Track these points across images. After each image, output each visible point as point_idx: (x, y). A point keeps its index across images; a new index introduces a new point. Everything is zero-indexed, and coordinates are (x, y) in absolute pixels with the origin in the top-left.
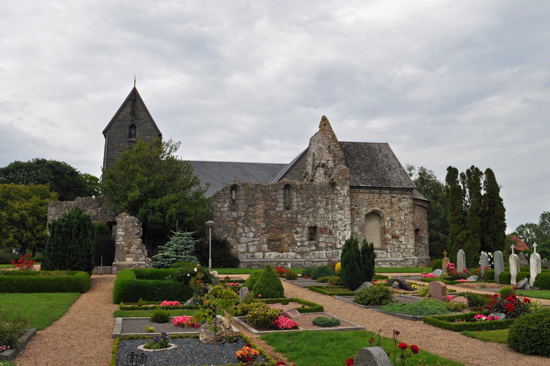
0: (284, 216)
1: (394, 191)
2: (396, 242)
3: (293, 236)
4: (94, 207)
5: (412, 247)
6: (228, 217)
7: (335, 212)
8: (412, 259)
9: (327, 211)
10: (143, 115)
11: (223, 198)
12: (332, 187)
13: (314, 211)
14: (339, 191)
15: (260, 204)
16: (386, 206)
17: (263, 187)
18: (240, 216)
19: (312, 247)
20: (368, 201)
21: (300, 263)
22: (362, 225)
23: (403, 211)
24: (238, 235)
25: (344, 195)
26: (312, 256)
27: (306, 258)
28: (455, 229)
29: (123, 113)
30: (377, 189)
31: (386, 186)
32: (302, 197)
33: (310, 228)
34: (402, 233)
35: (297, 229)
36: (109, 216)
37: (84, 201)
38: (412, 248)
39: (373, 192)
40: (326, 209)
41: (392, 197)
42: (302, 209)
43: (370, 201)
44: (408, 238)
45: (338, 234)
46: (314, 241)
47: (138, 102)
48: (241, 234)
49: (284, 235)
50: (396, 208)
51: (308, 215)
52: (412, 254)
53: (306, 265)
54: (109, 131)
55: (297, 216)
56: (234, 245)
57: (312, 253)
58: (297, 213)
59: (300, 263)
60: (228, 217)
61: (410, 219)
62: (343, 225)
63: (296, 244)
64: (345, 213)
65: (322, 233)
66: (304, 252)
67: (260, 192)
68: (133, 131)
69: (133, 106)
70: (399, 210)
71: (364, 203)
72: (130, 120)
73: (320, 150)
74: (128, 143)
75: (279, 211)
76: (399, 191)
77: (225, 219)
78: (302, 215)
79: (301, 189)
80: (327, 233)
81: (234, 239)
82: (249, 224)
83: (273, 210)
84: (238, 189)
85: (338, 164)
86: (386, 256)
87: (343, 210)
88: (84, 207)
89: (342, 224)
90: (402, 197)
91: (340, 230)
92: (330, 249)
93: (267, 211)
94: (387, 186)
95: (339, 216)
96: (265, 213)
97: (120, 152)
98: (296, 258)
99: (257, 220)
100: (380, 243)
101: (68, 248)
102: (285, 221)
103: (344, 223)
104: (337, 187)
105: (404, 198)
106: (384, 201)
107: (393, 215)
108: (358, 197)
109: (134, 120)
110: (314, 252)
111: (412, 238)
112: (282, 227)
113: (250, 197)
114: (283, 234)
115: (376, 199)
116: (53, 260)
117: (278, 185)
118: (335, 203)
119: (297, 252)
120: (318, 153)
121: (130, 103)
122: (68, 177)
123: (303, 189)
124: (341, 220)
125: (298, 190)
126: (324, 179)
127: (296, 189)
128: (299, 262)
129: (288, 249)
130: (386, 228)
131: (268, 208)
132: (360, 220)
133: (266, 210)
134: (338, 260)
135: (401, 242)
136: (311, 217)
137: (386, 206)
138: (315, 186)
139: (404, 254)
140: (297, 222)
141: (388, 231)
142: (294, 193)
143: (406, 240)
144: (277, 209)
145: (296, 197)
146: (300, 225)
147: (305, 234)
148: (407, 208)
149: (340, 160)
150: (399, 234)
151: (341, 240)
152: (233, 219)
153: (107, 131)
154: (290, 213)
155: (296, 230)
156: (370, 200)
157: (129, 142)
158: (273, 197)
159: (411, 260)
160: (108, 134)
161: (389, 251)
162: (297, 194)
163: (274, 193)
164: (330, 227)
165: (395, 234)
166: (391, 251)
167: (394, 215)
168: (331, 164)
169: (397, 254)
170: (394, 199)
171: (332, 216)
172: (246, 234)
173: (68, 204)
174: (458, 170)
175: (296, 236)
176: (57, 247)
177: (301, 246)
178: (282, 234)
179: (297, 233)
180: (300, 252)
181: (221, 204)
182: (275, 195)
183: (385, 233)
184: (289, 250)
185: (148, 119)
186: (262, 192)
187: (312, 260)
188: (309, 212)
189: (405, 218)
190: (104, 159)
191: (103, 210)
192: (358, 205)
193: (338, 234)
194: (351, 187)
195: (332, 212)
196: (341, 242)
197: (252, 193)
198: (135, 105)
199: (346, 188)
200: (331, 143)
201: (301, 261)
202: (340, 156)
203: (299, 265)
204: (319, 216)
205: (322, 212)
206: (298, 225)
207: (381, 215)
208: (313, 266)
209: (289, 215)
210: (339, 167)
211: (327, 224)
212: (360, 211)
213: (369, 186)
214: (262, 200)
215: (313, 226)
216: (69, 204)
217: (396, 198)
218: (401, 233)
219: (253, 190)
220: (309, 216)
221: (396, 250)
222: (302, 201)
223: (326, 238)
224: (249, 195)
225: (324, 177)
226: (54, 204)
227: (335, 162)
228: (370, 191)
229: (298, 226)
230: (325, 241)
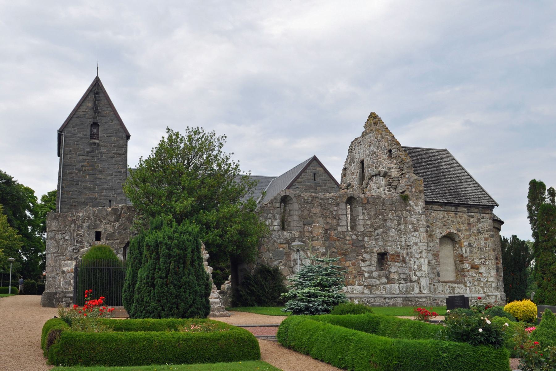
0: (348, 238)
1: (472, 209)
2: (476, 273)
3: (359, 264)
4: (109, 221)
5: (493, 280)
6: (279, 237)
7: (409, 234)
8: (494, 295)
9: (400, 233)
10: (108, 112)
11: (272, 212)
12: (405, 202)
13: (384, 232)
14: (413, 207)
15: (318, 222)
16: (464, 228)
17: (321, 199)
18: (294, 237)
19: (382, 279)
20: (442, 220)
21: (369, 300)
22: (437, 252)
23: (483, 234)
24: (292, 263)
25: (419, 212)
26: (382, 291)
27: (376, 294)
28: (548, 258)
29: (83, 108)
30: (453, 206)
31: (464, 203)
32: (369, 214)
33: (378, 254)
34: (483, 262)
35: (364, 255)
36: (130, 234)
37: (96, 212)
38: (494, 282)
39: (449, 210)
40: (398, 230)
41: (470, 216)
42: (370, 229)
43: (445, 221)
44: (489, 268)
45: (412, 262)
46: (384, 271)
47: (101, 96)
48: (295, 260)
49: (348, 263)
50: (474, 229)
51: (377, 237)
52: (494, 289)
53: (376, 302)
54: (66, 129)
55: (364, 238)
56: (287, 275)
57: (382, 287)
58: (364, 235)
59: (369, 300)
60: (279, 237)
61: (491, 245)
62: (419, 251)
63: (363, 274)
64: (420, 235)
65: (394, 260)
66: (373, 286)
67: (318, 206)
68: (95, 131)
69: (96, 99)
70: (478, 233)
71: (438, 223)
72: (91, 117)
73: (374, 155)
74: (89, 145)
75: (342, 231)
76: (477, 210)
77: (275, 241)
78: (369, 237)
79: (367, 203)
80: (400, 261)
81: (286, 268)
82: (306, 248)
83: (335, 230)
84: (290, 202)
85: (408, 172)
86: (464, 291)
87: (417, 232)
88: (96, 221)
89: (417, 249)
90: (481, 216)
91: (415, 257)
92: (403, 282)
93: (327, 232)
94: (466, 203)
95: (413, 239)
96: (325, 234)
97: (80, 156)
98: (363, 293)
99: (315, 242)
100: (454, 275)
101: (182, 281)
102: (349, 244)
103: (419, 248)
104: (410, 202)
105: (483, 218)
106: (460, 221)
107: (472, 239)
108: (431, 216)
109: (97, 117)
110: (385, 286)
111: (493, 269)
112: (346, 252)
113: (306, 212)
114: (347, 262)
115: (451, 219)
116: (159, 301)
117: (340, 197)
118: (409, 223)
119: (365, 286)
120: (371, 159)
121: (92, 96)
122: (5, 187)
123: (370, 203)
124: (416, 244)
125: (364, 204)
126: (386, 192)
127: (362, 203)
128: (368, 298)
129: (353, 282)
130: (464, 255)
131: (328, 227)
132: (433, 244)
133: (326, 230)
134: (413, 296)
135: (481, 273)
136: (380, 239)
137: (464, 228)
138: (384, 200)
139: (485, 289)
140: (363, 247)
141: (466, 259)
142: (359, 208)
143: (487, 271)
144: (339, 229)
145: (362, 214)
146: (368, 250)
147: (373, 262)
148: (487, 231)
149: (409, 167)
150: (479, 264)
151: (416, 270)
152: (285, 242)
153: (63, 130)
154: (355, 235)
155: (362, 256)
156: (445, 219)
157: (91, 144)
158: (334, 213)
159: (494, 297)
160: (65, 133)
161: (468, 285)
162: (362, 210)
163: (336, 208)
164: (403, 254)
165: (474, 263)
166: (470, 285)
167: (472, 239)
168: (394, 173)
169: (477, 289)
170: (472, 220)
171: (405, 240)
172: (301, 261)
173: (74, 216)
174: (546, 184)
175: (362, 264)
176: (165, 280)
177: (369, 277)
178: (345, 262)
179: (364, 260)
180: (368, 285)
181: (270, 221)
182: (336, 211)
183: (462, 262)
184: (355, 283)
185: (114, 116)
186: (320, 206)
187: (383, 296)
188: (377, 233)
189: (485, 243)
190: (60, 165)
191: (121, 225)
192: (430, 226)
193: (412, 262)
194: (427, 203)
195: (406, 235)
196: (417, 273)
197: (308, 207)
198: (97, 97)
199: (421, 203)
200: (393, 146)
201: (370, 298)
202: (409, 162)
203: (367, 302)
204: (390, 239)
205: (393, 234)
206: (365, 250)
207: (457, 239)
208: (385, 304)
209: (354, 237)
210: (409, 176)
211: (399, 250)
212: (434, 233)
213: (445, 201)
214: (320, 217)
215: (383, 251)
216: (75, 217)
217: (475, 218)
218: (481, 263)
219: (308, 203)
220: (378, 239)
221: (476, 283)
222: (369, 219)
223: (398, 268)
224: (304, 210)
225: (387, 189)
226: (55, 217)
227: (402, 170)
228: (445, 208)
229: (365, 252)
230: (398, 271)
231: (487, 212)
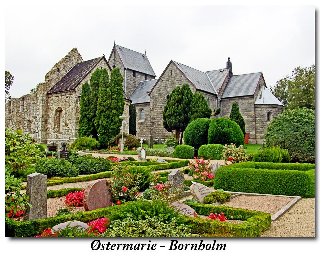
45: (37, 124)
159: (72, 141)
170: (67, 99)
231: (73, 93)
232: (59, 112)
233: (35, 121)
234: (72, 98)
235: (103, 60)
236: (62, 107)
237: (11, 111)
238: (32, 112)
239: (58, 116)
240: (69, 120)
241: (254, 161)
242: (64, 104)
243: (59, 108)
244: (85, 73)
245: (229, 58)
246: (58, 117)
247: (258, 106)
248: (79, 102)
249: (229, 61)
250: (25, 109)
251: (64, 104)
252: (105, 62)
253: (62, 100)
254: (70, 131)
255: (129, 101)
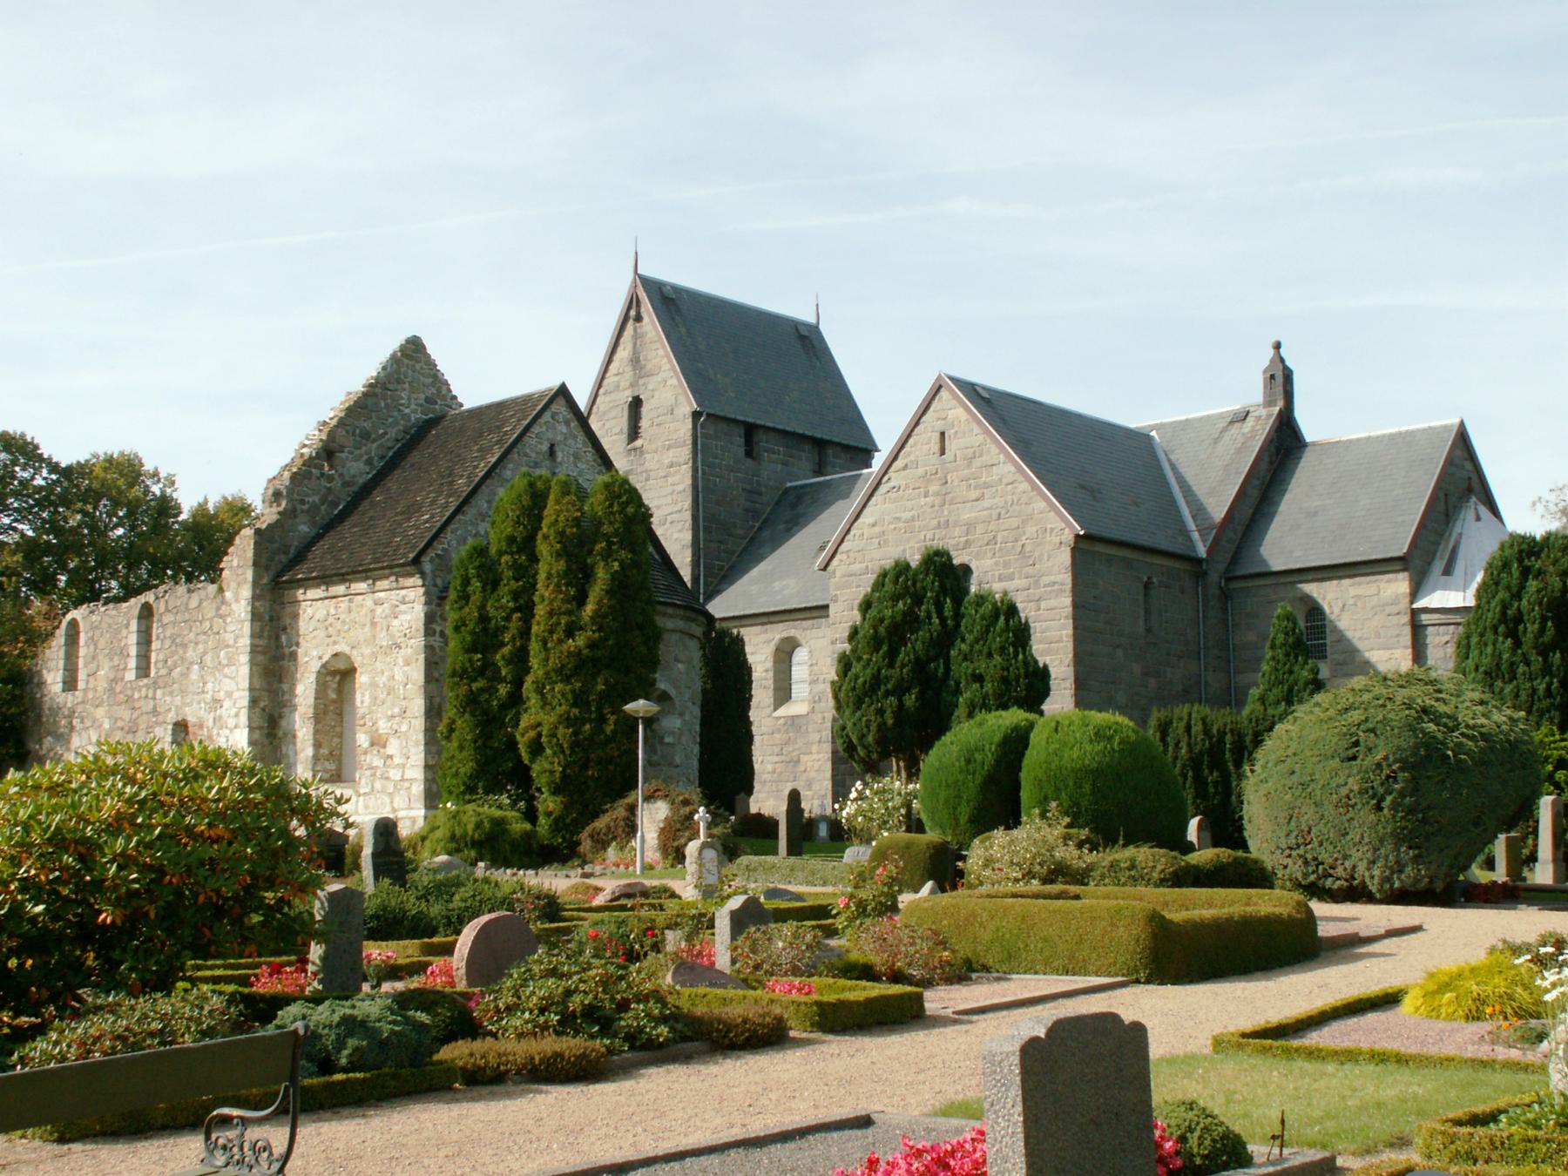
170: (379, 610)
232: (338, 678)
233: (211, 723)
234: (403, 607)
235: (560, 407)
236: (354, 652)
237: (82, 675)
238: (194, 676)
239: (333, 696)
240: (393, 717)
241: (1283, 888)
242: (361, 638)
243: (336, 655)
244: (469, 477)
245: (1278, 346)
246: (334, 701)
247: (1436, 616)
248: (438, 629)
249: (1282, 360)
250: (160, 665)
251: (361, 638)
252: (570, 416)
253: (354, 614)
254: (395, 774)
255: (693, 615)
